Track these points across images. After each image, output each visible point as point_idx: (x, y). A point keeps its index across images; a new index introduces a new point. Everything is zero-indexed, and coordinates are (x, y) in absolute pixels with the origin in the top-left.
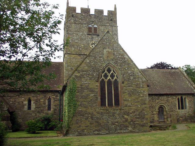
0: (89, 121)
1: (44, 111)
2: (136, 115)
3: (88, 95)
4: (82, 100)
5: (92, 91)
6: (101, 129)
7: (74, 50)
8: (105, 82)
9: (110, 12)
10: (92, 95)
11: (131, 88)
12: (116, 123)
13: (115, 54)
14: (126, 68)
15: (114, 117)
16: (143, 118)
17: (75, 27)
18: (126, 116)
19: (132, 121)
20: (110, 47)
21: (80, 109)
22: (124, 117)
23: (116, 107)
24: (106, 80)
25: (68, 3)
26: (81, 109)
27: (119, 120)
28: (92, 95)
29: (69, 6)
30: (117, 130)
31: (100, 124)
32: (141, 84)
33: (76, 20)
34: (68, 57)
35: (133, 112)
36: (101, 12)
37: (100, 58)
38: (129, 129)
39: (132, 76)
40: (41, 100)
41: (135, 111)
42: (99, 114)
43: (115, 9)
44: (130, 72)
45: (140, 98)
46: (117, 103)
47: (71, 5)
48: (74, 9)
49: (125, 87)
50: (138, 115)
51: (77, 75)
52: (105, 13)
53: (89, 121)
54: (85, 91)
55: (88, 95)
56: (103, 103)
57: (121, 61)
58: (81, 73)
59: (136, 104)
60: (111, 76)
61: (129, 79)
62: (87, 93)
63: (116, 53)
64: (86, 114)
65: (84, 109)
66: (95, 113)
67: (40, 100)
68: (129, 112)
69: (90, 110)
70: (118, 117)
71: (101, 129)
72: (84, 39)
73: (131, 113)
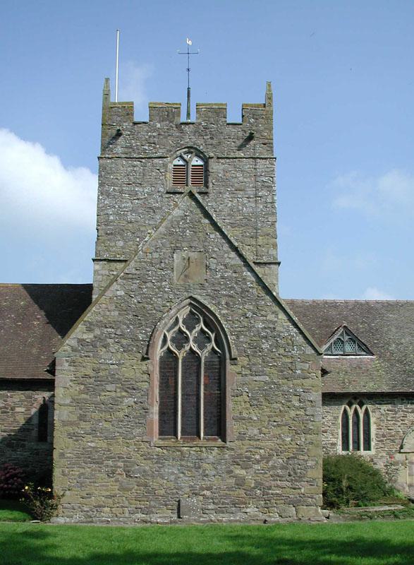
0: (117, 481)
1: (26, 443)
2: (274, 467)
3: (116, 402)
4: (97, 415)
5: (131, 388)
6: (155, 507)
7: (123, 248)
8: (176, 358)
9: (250, 112)
10: (130, 401)
11: (261, 378)
12: (205, 492)
13: (213, 267)
14: (249, 314)
15: (201, 471)
16: (300, 478)
17: (129, 169)
18: (239, 472)
19: (259, 485)
20: (194, 244)
21: (92, 442)
22: (232, 471)
23: (208, 440)
24: (181, 355)
25: (107, 95)
26: (92, 445)
27: (215, 482)
28: (130, 401)
29: (112, 100)
30: (207, 512)
31: (153, 492)
32: (298, 367)
33: (131, 147)
34: (104, 272)
35: (263, 458)
36: (220, 111)
37: (161, 280)
38: (248, 510)
39: (266, 337)
40: (18, 409)
41: (271, 456)
42: (149, 462)
43: (269, 98)
44: (260, 325)
45: (293, 414)
46: (219, 428)
47: (116, 98)
48: (127, 109)
49: (239, 377)
50: (283, 468)
51: (85, 336)
52: (234, 116)
53: (117, 481)
54: (109, 387)
55: (116, 402)
56: (167, 427)
57: (232, 288)
58: (97, 332)
59: (277, 431)
60: (187, 339)
61: (256, 348)
62: (113, 394)
63: (217, 264)
64: (108, 458)
65: (103, 444)
66: (136, 457)
67: (12, 409)
68: (249, 458)
69: (119, 449)
70: (214, 472)
71: (155, 507)
72: (158, 208)
73: (258, 462)
